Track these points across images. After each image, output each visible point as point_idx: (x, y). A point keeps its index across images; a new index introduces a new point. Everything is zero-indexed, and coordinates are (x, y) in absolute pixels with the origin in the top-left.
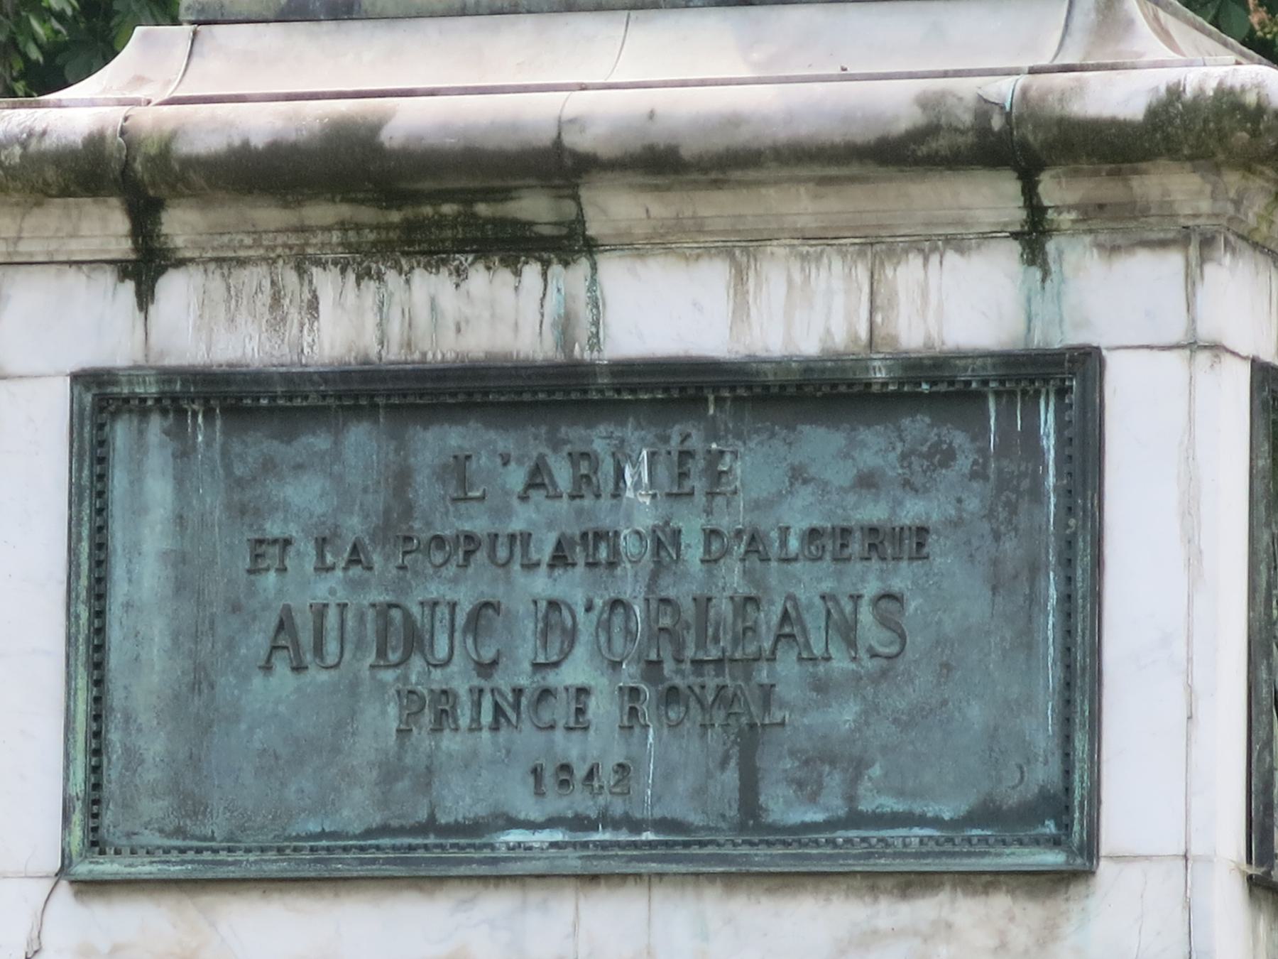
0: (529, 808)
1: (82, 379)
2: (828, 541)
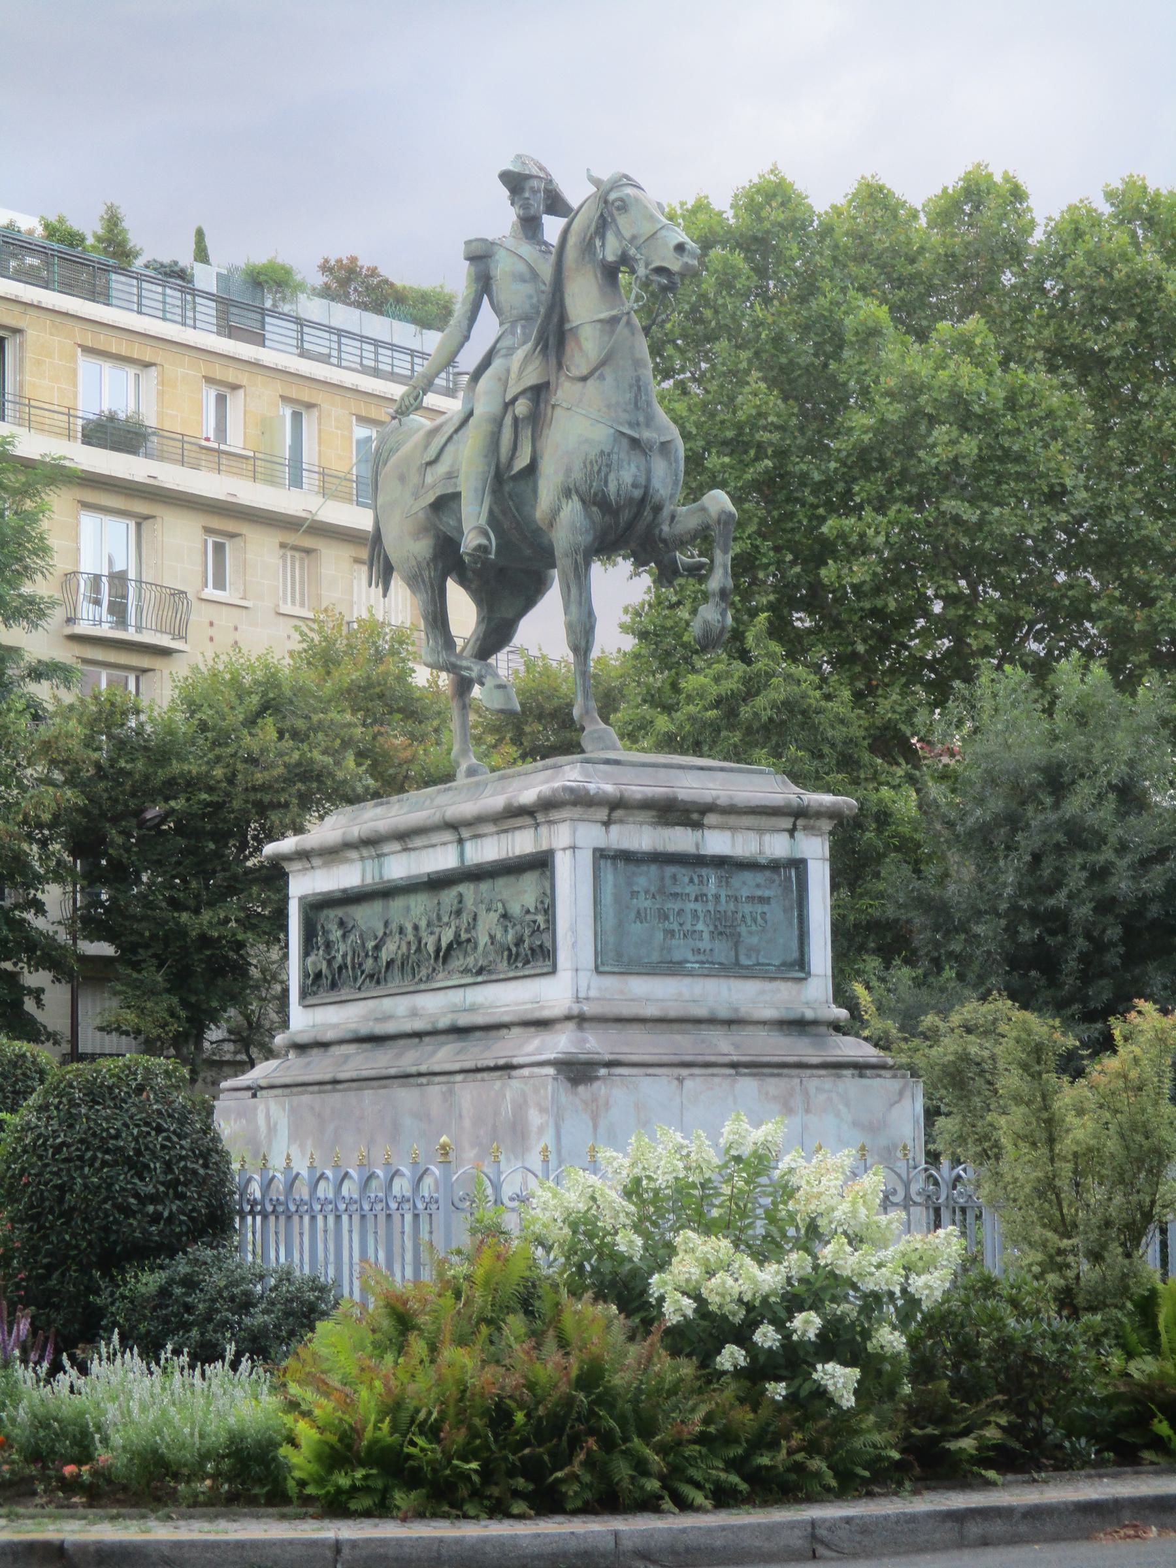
0: (692, 959)
1: (595, 850)
2: (750, 899)
